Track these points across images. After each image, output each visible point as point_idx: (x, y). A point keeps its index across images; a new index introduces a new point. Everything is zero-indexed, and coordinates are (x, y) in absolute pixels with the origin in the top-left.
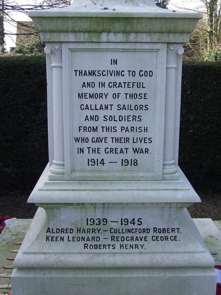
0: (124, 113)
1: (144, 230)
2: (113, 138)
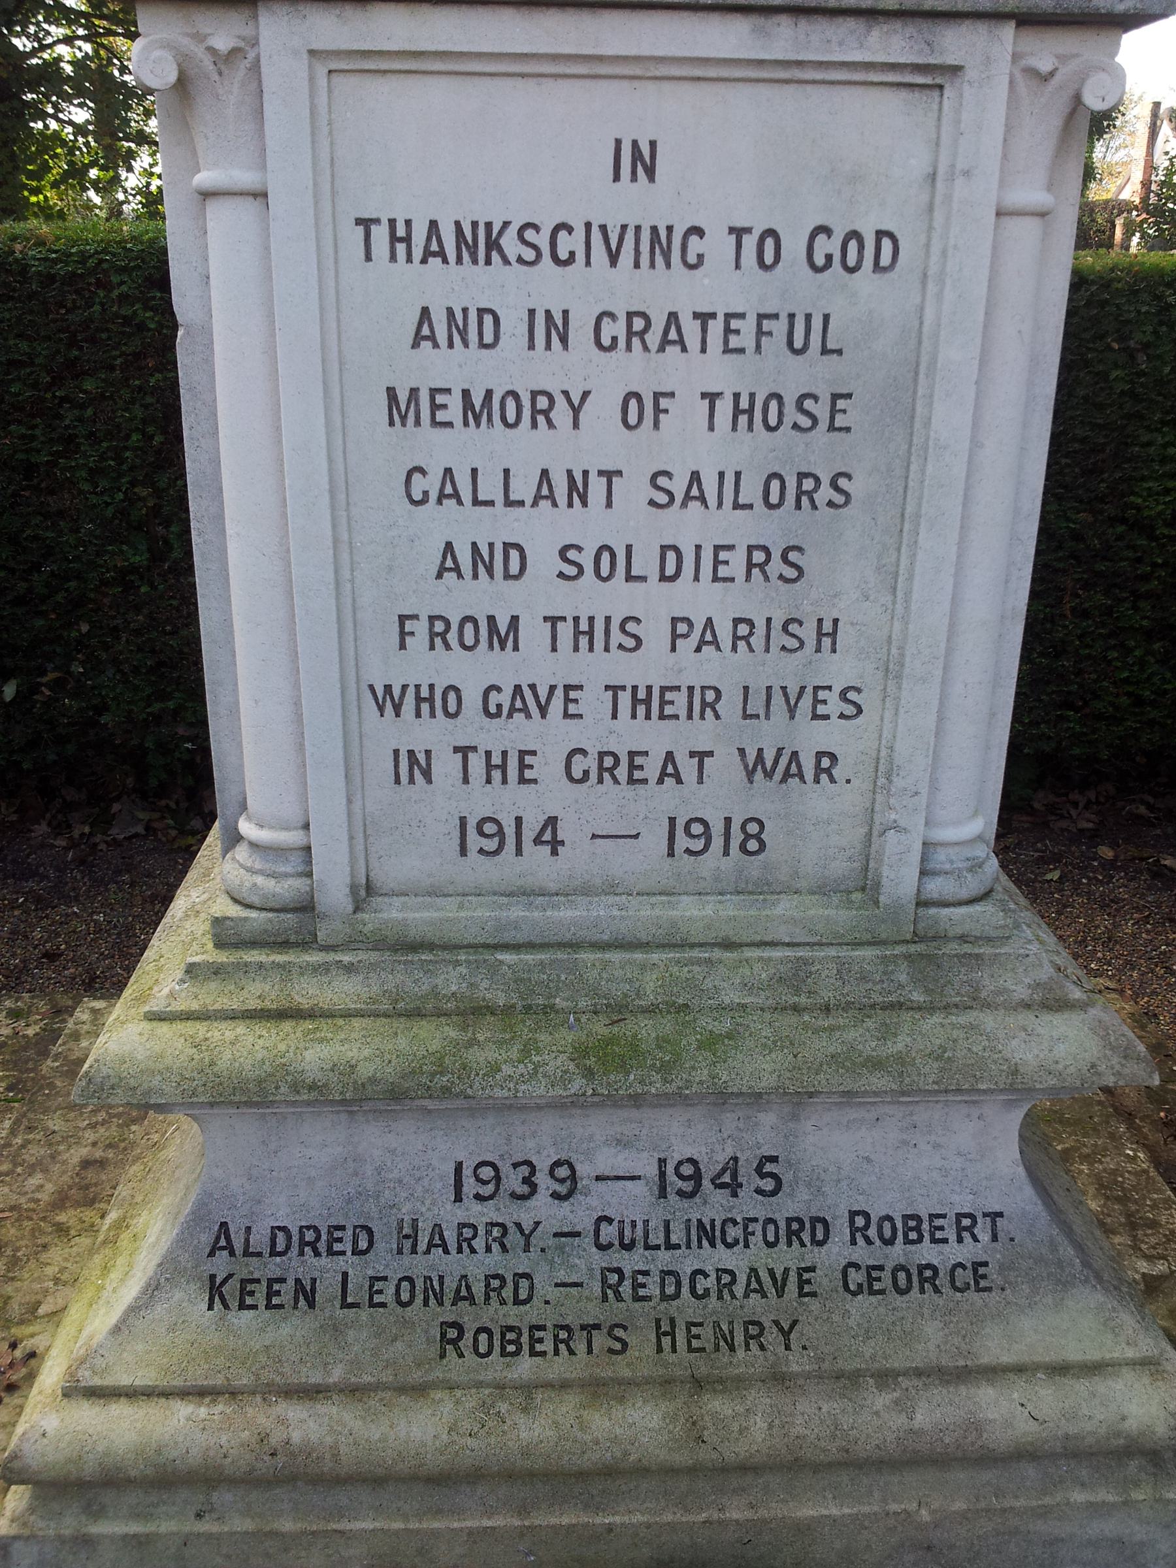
0: (690, 527)
1: (795, 1226)
2: (614, 689)
